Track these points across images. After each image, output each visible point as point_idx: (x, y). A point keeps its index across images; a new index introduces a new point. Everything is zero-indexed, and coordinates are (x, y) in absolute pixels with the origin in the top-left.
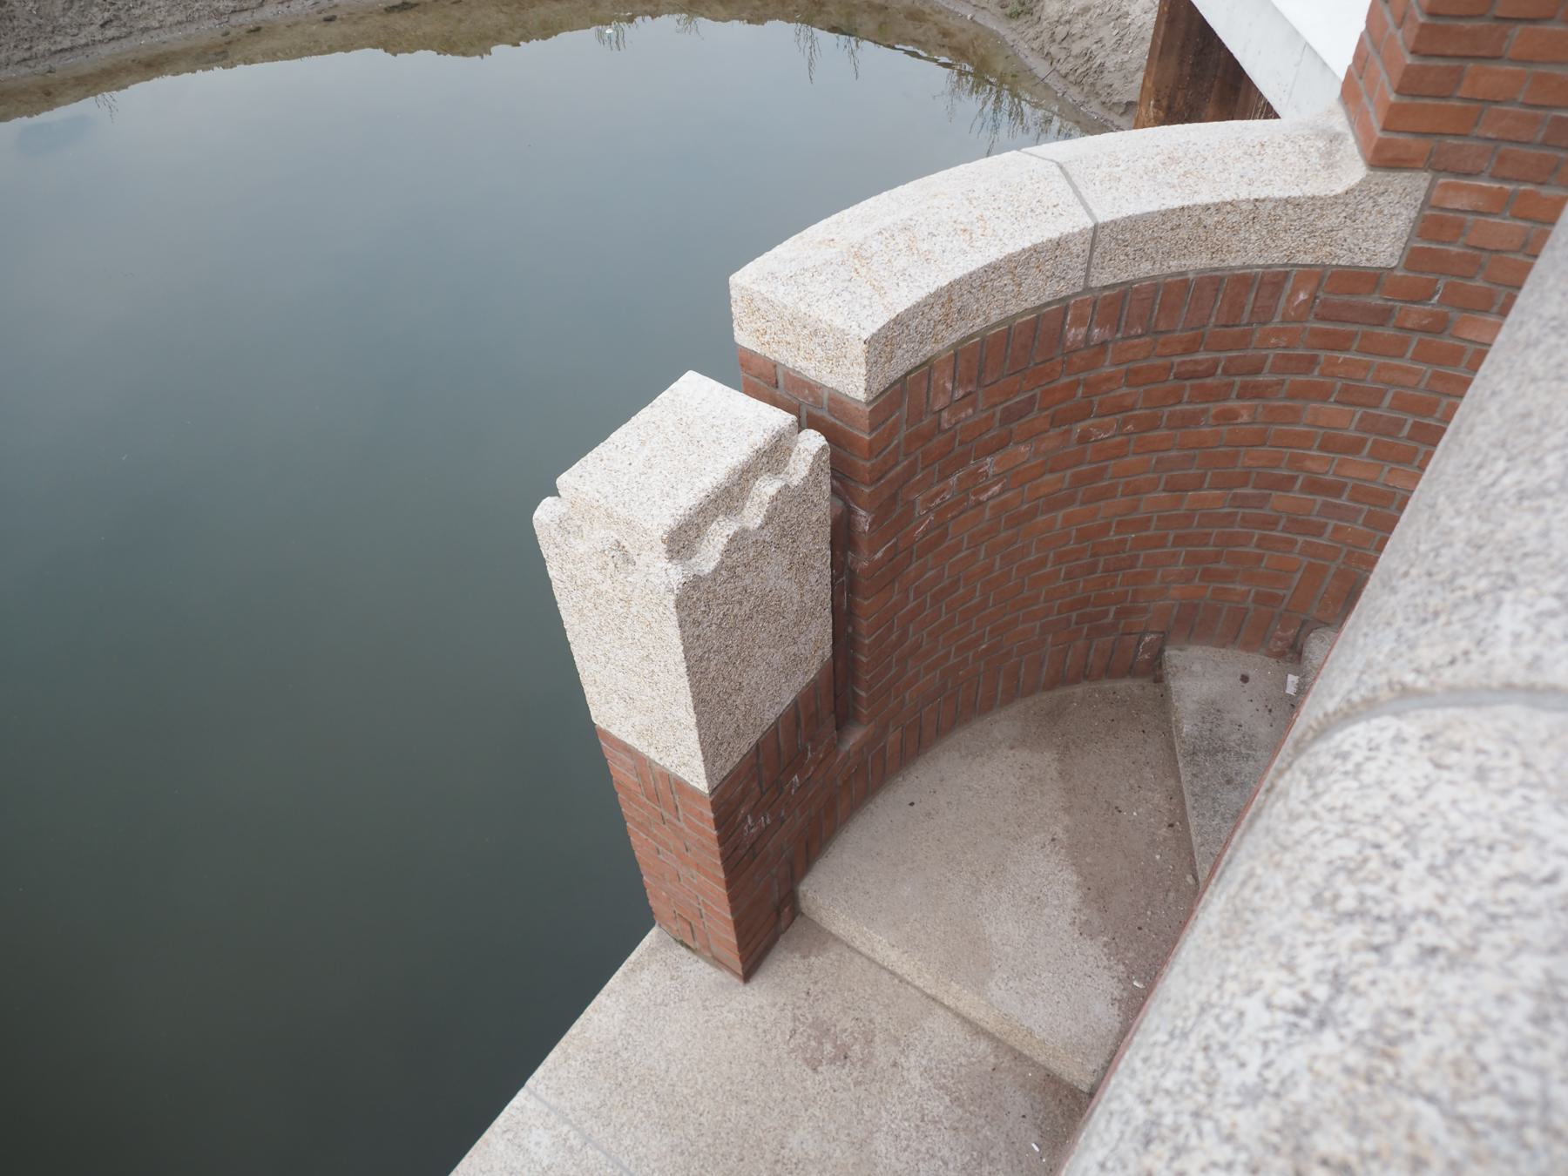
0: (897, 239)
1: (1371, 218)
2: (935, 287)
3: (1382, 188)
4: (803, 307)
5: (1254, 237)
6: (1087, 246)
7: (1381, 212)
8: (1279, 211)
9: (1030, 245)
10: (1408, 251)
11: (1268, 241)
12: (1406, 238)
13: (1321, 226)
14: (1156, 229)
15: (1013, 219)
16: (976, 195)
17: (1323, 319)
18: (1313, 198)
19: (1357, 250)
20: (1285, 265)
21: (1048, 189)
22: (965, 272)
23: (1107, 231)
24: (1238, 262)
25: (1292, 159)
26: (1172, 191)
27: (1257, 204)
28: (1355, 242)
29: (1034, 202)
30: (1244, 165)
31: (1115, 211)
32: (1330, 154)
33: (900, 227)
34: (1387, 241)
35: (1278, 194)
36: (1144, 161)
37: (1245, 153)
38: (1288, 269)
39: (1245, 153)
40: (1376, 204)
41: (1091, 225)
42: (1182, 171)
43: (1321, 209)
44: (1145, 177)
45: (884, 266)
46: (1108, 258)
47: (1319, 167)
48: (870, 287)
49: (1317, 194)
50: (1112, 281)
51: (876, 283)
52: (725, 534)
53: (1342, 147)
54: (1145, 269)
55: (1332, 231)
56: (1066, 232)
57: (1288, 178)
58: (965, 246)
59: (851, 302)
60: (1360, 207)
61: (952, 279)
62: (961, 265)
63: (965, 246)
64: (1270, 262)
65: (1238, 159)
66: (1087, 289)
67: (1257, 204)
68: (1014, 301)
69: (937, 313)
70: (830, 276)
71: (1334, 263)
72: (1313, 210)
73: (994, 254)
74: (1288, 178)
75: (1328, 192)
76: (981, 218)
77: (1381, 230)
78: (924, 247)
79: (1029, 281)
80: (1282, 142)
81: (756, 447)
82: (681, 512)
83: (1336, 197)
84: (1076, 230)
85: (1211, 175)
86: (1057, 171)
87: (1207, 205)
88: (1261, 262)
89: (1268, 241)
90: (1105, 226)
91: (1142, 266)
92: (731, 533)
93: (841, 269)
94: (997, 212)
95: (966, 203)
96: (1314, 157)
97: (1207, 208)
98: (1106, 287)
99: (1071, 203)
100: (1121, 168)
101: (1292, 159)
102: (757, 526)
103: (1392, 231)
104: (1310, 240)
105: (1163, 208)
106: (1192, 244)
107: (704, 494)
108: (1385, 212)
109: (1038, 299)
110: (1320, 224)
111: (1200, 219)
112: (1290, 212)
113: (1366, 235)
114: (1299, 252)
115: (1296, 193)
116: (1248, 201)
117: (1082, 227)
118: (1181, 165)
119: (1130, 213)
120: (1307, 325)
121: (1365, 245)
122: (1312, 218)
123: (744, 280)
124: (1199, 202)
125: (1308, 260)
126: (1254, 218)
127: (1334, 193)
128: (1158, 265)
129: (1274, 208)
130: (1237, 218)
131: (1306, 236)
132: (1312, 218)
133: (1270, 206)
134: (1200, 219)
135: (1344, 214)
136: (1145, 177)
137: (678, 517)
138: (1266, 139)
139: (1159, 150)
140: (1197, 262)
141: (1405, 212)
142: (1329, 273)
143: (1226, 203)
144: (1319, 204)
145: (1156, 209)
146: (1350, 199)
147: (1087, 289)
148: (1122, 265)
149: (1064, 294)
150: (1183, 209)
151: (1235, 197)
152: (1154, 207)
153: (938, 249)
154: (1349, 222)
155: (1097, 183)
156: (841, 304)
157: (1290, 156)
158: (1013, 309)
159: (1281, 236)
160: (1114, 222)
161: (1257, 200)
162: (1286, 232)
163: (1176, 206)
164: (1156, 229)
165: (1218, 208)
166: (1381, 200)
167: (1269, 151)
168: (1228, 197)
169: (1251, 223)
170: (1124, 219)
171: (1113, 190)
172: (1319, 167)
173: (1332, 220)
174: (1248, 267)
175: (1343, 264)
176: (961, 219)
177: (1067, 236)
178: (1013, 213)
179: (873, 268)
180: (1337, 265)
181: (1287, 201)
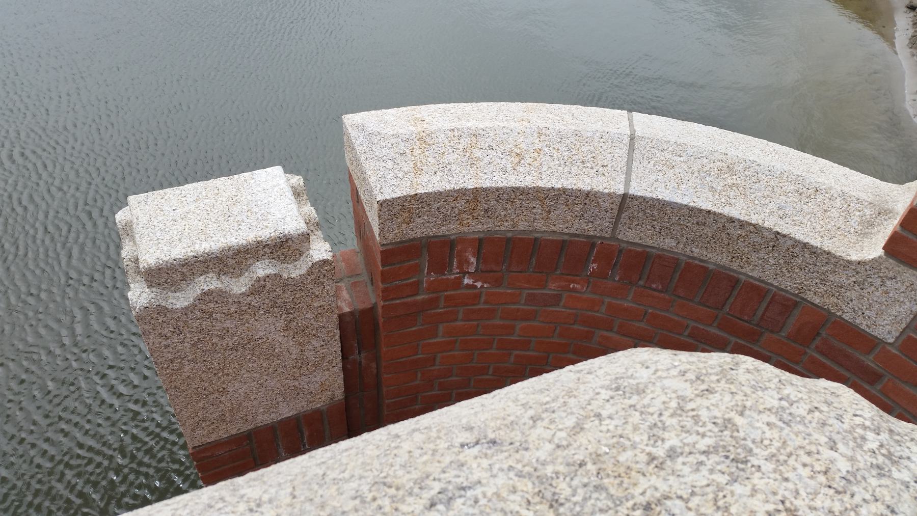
0: (462, 141)
1: (877, 294)
2: (462, 186)
3: (891, 274)
4: (363, 158)
5: (772, 261)
6: (616, 207)
7: (887, 293)
8: (797, 250)
9: (560, 186)
10: (904, 337)
11: (784, 270)
12: (904, 325)
13: (832, 279)
14: (682, 218)
15: (562, 162)
16: (548, 132)
17: (822, 353)
18: (829, 253)
19: (860, 313)
20: (797, 295)
21: (609, 151)
22: (493, 185)
23: (636, 203)
24: (755, 274)
25: (834, 213)
26: (710, 194)
27: (778, 236)
28: (860, 306)
29: (589, 157)
30: (788, 200)
31: (649, 190)
32: (871, 224)
33: (471, 132)
34: (888, 320)
35: (799, 236)
36: (705, 161)
37: (797, 191)
38: (798, 300)
39: (797, 191)
40: (883, 284)
41: (621, 190)
42: (730, 182)
43: (835, 266)
44: (696, 174)
45: (436, 155)
46: (636, 223)
47: (852, 230)
48: (412, 166)
49: (833, 252)
50: (637, 241)
51: (419, 165)
52: (202, 288)
53: (885, 223)
54: (668, 243)
55: (841, 287)
56: (596, 189)
57: (818, 227)
58: (509, 166)
59: (389, 169)
60: (869, 280)
61: (480, 186)
62: (494, 179)
63: (509, 166)
64: (783, 287)
65: (786, 194)
66: (613, 237)
67: (778, 236)
68: (543, 221)
69: (461, 204)
70: (390, 145)
71: (838, 314)
72: (827, 263)
73: (528, 181)
74: (818, 227)
75: (843, 255)
76: (539, 151)
77: (884, 307)
78: (477, 153)
79: (558, 212)
80: (835, 195)
81: (259, 239)
82: (166, 259)
83: (849, 262)
84: (606, 191)
85: (753, 196)
86: (627, 140)
87: (731, 218)
88: (775, 283)
89: (784, 270)
90: (634, 198)
91: (666, 240)
92: (207, 288)
93: (403, 144)
94: (555, 152)
95: (536, 135)
96: (854, 221)
97: (732, 220)
98: (628, 242)
99: (618, 169)
100: (682, 159)
101: (834, 213)
102: (240, 292)
103: (894, 313)
104: (821, 286)
105: (692, 204)
106: (715, 242)
107: (193, 254)
108: (891, 295)
109: (567, 228)
110: (831, 277)
111: (724, 226)
112: (807, 255)
113: (870, 305)
114: (809, 290)
115: (815, 242)
116: (770, 230)
117: (612, 191)
118: (734, 177)
119: (660, 197)
120: (808, 351)
121: (867, 313)
122: (825, 269)
123: (351, 120)
124: (726, 213)
125: (817, 301)
126: (774, 246)
127: (849, 258)
128: (681, 246)
129: (793, 246)
130: (759, 239)
131: (818, 281)
132: (825, 269)
133: (789, 243)
134: (724, 226)
135: (854, 279)
136: (696, 174)
137: (161, 262)
138: (822, 188)
139: (724, 158)
140: (717, 258)
141: (908, 303)
142: (833, 320)
143: (750, 224)
144: (833, 260)
145: (685, 203)
146: (860, 269)
147: (613, 237)
148: (649, 233)
149: (591, 233)
150: (709, 212)
151: (760, 222)
152: (685, 201)
153: (486, 160)
154: (857, 288)
155: (652, 162)
156: (381, 169)
157: (833, 210)
158: (539, 225)
159: (797, 271)
160: (644, 199)
161: (778, 233)
162: (801, 269)
163: (703, 208)
164: (682, 218)
165: (743, 224)
166: (888, 283)
167: (820, 198)
168: (754, 219)
169: (770, 248)
170: (652, 199)
171: (660, 174)
172: (852, 230)
173: (841, 278)
174: (763, 281)
175: (846, 318)
176: (523, 146)
177: (596, 193)
178: (566, 158)
179: (427, 153)
180: (840, 317)
181: (805, 246)
